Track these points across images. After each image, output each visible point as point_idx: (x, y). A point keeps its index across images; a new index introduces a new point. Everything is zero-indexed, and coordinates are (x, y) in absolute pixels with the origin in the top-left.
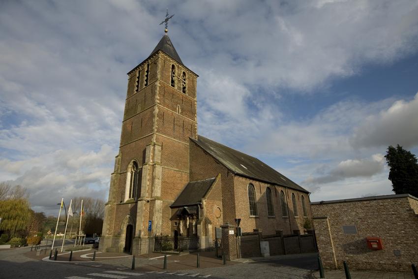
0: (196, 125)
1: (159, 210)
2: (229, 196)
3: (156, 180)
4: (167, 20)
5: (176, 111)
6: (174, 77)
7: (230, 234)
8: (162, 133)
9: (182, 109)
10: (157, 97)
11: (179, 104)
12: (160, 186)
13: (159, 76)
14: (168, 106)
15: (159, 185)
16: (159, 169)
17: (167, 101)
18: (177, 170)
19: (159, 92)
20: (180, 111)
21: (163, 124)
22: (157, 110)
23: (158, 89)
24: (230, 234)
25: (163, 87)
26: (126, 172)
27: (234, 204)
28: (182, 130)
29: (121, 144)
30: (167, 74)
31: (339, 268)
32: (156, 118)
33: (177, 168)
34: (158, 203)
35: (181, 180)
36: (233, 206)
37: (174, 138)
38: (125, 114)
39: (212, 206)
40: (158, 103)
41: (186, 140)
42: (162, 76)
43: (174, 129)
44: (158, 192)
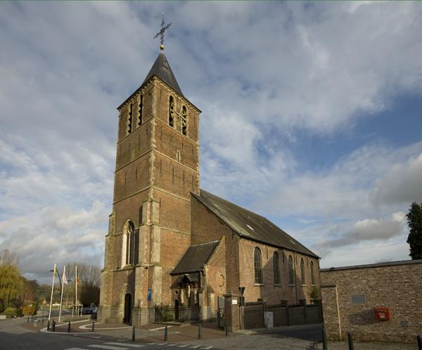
4: (162, 31)
8: (160, 187)
10: (154, 140)
21: (161, 176)
26: (122, 234)
28: (182, 182)
29: (115, 200)
32: (153, 168)
34: (158, 269)
44: (157, 258)
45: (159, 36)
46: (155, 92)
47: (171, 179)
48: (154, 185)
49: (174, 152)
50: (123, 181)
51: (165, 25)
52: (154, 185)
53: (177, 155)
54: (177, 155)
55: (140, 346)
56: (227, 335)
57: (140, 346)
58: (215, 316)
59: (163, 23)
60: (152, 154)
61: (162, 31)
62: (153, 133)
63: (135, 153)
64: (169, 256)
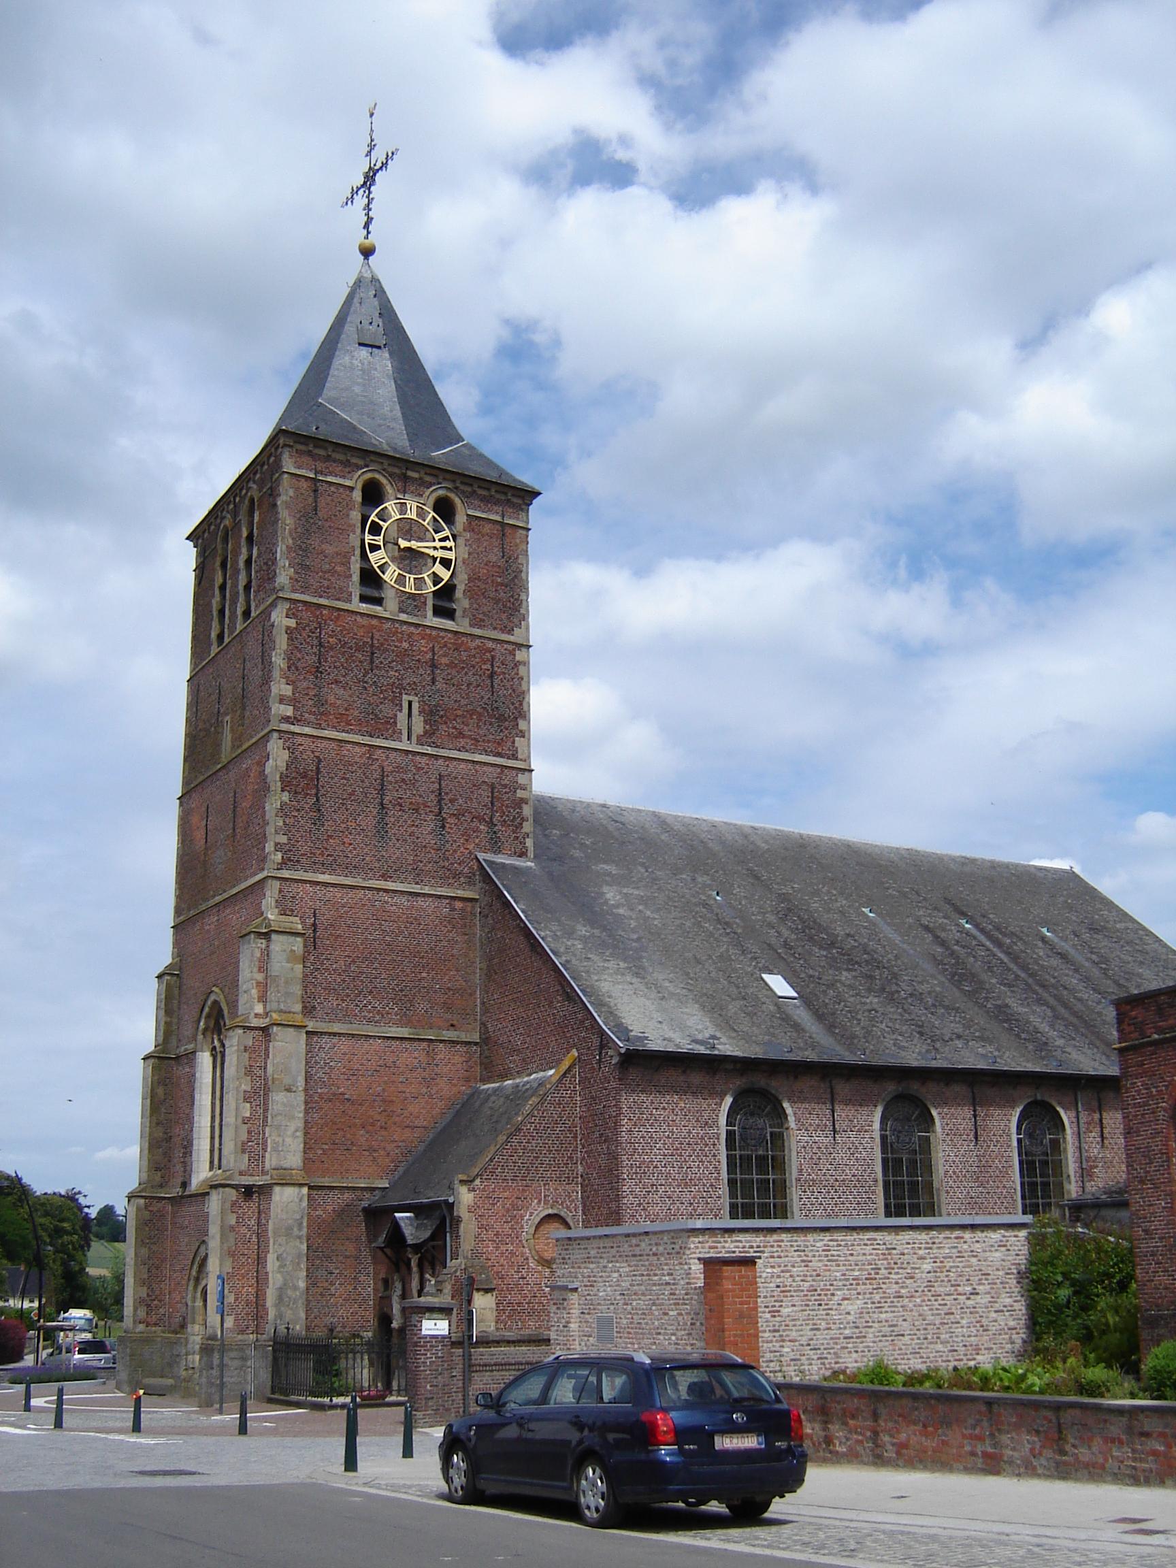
0: (522, 779)
1: (290, 1228)
2: (602, 1161)
3: (278, 1099)
4: (370, 178)
5: (396, 735)
6: (374, 548)
7: (424, 1332)
8: (316, 866)
9: (430, 714)
10: (280, 688)
11: (413, 688)
12: (297, 1123)
13: (283, 577)
14: (343, 721)
15: (292, 1118)
16: (288, 1049)
17: (336, 696)
18: (404, 1032)
19: (289, 657)
20: (419, 726)
21: (318, 821)
22: (277, 757)
23: (282, 642)
24: (424, 1332)
25: (313, 624)
26: (194, 1053)
27: (618, 1198)
28: (430, 824)
29: (178, 911)
30: (329, 549)
31: (60, 1393)
32: (276, 799)
33: (405, 1021)
34: (287, 1202)
35: (428, 1082)
36: (613, 1205)
37: (385, 877)
38: (185, 760)
39: (515, 1207)
40: (286, 719)
41: (456, 875)
42: (302, 567)
43: (382, 829)
44: (286, 1147)
45: (360, 200)
46: (286, 493)
47: (368, 821)
48: (283, 865)
49: (386, 710)
50: (199, 835)
51: (379, 155)
52: (283, 865)
53: (402, 717)
54: (402, 717)
55: (664, 1505)
56: (243, 1429)
57: (664, 1505)
58: (358, 1355)
59: (372, 147)
60: (276, 747)
61: (370, 178)
62: (278, 660)
63: (232, 730)
64: (362, 1136)
